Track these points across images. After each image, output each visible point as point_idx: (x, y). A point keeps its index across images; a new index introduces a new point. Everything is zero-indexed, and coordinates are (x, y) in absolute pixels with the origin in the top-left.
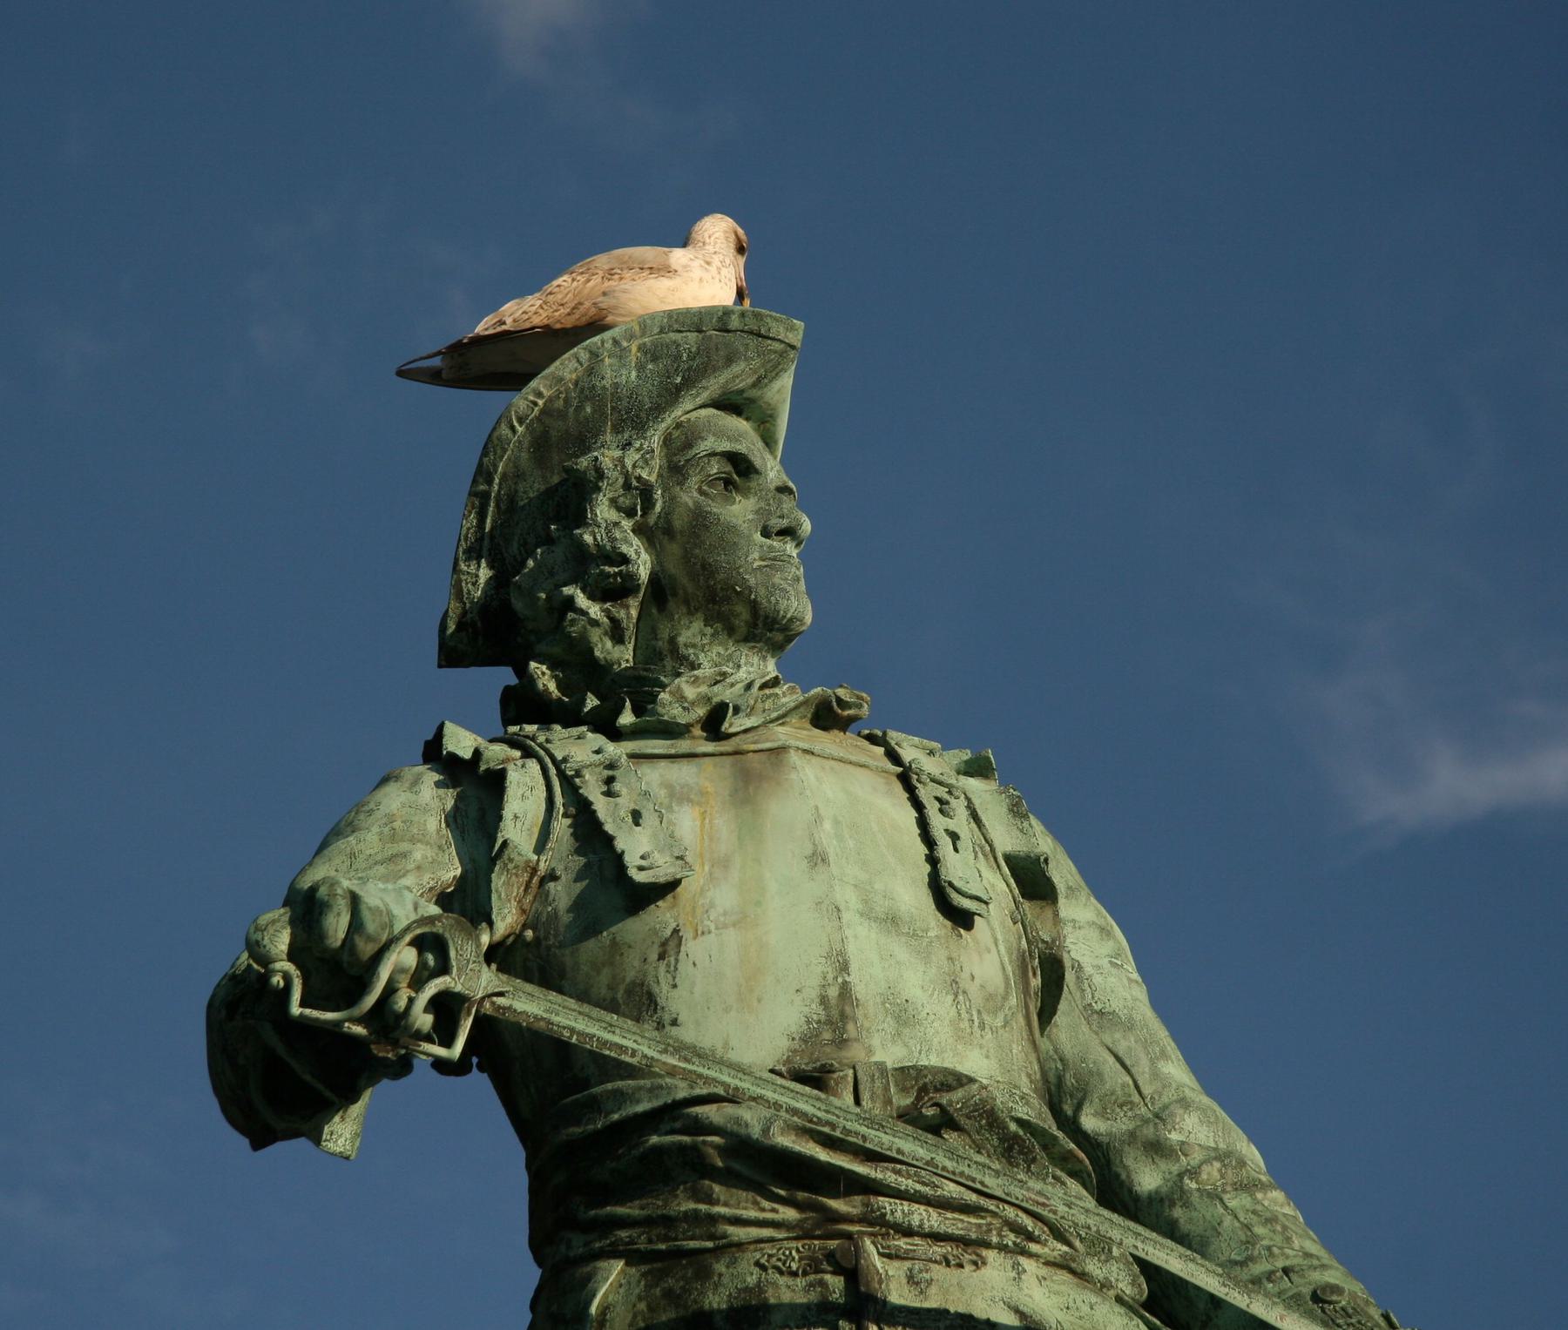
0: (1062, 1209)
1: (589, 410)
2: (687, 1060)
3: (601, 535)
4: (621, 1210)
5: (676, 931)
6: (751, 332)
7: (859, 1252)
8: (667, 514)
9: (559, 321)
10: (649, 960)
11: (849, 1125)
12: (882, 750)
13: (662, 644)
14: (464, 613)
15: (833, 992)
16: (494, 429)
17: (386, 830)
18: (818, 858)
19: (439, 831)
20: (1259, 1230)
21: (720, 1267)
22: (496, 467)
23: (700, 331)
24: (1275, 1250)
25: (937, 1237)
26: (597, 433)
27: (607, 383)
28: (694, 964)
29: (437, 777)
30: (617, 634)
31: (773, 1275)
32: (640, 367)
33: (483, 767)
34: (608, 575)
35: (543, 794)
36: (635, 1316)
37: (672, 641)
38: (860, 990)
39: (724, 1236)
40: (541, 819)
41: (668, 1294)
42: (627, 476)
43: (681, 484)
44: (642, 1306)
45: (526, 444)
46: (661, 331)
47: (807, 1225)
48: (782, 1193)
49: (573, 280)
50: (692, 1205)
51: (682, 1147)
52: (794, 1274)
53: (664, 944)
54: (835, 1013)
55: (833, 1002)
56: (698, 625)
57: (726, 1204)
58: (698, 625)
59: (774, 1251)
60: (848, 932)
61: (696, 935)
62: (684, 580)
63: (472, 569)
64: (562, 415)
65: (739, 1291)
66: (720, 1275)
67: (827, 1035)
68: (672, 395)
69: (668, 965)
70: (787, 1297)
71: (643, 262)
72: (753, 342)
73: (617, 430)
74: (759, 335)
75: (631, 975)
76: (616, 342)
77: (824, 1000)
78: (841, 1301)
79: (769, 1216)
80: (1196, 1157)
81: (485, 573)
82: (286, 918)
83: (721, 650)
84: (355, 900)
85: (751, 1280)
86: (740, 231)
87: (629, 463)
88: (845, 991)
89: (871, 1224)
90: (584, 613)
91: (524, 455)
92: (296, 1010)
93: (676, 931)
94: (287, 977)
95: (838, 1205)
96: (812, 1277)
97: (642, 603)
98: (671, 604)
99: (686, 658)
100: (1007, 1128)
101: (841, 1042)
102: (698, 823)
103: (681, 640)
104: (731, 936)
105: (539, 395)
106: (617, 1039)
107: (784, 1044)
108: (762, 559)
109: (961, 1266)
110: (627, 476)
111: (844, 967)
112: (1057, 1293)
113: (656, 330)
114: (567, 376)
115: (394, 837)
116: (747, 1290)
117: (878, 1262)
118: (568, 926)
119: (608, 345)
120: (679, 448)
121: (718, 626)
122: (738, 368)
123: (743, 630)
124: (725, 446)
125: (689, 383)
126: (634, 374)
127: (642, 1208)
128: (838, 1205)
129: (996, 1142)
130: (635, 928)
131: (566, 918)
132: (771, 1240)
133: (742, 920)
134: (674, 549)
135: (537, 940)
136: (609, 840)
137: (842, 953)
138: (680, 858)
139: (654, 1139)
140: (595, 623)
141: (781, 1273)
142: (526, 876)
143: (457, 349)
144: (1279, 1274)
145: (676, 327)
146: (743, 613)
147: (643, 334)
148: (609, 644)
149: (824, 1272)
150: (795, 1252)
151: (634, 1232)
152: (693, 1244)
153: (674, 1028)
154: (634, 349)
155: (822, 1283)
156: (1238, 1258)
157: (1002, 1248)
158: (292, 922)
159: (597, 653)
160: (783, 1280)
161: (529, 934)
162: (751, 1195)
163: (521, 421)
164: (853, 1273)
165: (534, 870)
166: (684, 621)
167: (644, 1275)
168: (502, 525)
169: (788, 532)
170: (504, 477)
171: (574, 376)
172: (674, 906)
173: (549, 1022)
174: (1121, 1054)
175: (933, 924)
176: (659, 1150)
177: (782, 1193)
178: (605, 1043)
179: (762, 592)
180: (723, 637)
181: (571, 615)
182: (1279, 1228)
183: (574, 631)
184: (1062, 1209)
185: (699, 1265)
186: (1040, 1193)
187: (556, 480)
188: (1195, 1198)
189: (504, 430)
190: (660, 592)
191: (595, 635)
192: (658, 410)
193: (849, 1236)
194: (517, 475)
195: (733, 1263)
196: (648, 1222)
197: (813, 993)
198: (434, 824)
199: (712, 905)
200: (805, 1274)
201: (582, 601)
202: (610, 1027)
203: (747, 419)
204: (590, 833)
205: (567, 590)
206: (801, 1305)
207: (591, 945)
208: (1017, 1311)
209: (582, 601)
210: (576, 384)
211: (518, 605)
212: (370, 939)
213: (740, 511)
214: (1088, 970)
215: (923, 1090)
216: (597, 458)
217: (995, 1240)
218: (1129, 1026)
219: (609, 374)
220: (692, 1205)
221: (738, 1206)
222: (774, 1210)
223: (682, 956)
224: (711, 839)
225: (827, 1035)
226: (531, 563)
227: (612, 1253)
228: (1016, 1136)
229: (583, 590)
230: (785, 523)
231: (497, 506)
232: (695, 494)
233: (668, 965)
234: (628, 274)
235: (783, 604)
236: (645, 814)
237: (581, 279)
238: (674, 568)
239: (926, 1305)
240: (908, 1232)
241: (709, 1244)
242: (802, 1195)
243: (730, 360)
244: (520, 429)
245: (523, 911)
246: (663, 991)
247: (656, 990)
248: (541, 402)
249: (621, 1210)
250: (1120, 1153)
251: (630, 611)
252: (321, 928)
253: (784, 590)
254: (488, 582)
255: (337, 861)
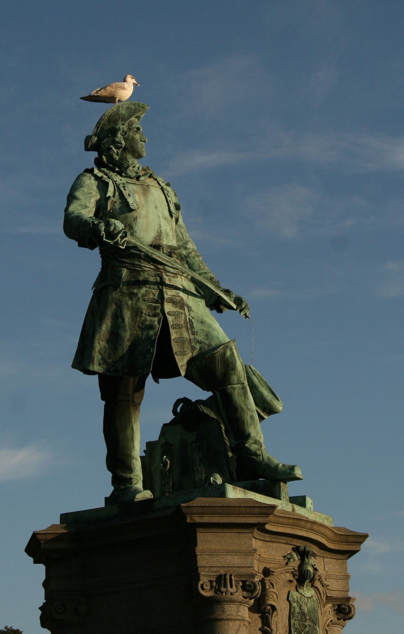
0: (197, 277)
1: (117, 116)
2: (153, 251)
3: (119, 140)
4: (126, 261)
5: (136, 217)
6: (143, 107)
7: (162, 275)
8: (128, 136)
9: (107, 95)
10: (132, 221)
11: (172, 263)
12: (156, 181)
13: (124, 157)
14: (92, 144)
15: (159, 231)
16: (102, 117)
17: (88, 188)
18: (156, 207)
19: (96, 189)
20: (201, 265)
21: (142, 273)
22: (101, 123)
23: (135, 106)
24: (204, 269)
25: (172, 273)
26: (118, 121)
27: (121, 112)
28: (139, 223)
29: (94, 178)
30: (117, 154)
31: (150, 276)
32: (126, 111)
33: (103, 179)
34: (119, 146)
35: (113, 187)
36: (128, 278)
37: (126, 157)
38: (163, 231)
39: (143, 269)
40: (113, 191)
41: (133, 276)
42: (123, 130)
43: (130, 132)
44: (129, 277)
45: (107, 120)
46: (129, 105)
47: (155, 269)
48: (152, 263)
49: (110, 88)
50: (138, 263)
51: (137, 254)
52: (153, 277)
53: (134, 219)
54: (159, 234)
55: (159, 232)
56: (130, 155)
57: (143, 264)
58: (130, 155)
59: (150, 273)
60: (161, 221)
61: (139, 218)
62: (130, 149)
63: (94, 138)
64: (113, 116)
65: (145, 278)
66: (142, 275)
67: (158, 238)
68: (130, 116)
69: (135, 223)
70: (151, 280)
71: (121, 86)
72: (142, 109)
73: (122, 121)
74: (144, 108)
75: (129, 223)
76: (122, 105)
77: (158, 232)
78: (159, 282)
79: (150, 267)
80: (191, 250)
81: (96, 139)
82: (104, 225)
83: (132, 159)
84: (115, 224)
85: (146, 276)
86: (130, 76)
88: (161, 230)
89: (164, 270)
90: (114, 151)
91: (106, 122)
92: (104, 240)
93: (136, 217)
94: (103, 234)
95: (159, 266)
96: (155, 277)
97: (122, 150)
98: (126, 151)
99: (128, 160)
100: (182, 256)
101: (160, 239)
102: (139, 198)
103: (127, 157)
104: (145, 219)
105: (110, 112)
106: (144, 247)
107: (152, 239)
108: (141, 146)
109: (175, 278)
110: (123, 130)
111: (160, 227)
112: (186, 282)
113: (128, 104)
114: (114, 110)
115: (89, 189)
116: (146, 278)
117: (165, 276)
118: (118, 212)
119: (121, 105)
120: (131, 125)
123: (136, 157)
125: (133, 115)
126: (125, 112)
127: (130, 261)
128: (159, 266)
129: (180, 258)
130: (129, 215)
131: (118, 210)
132: (150, 271)
133: (146, 217)
134: (128, 143)
135: (112, 212)
136: (126, 199)
137: (160, 224)
138: (137, 205)
139: (132, 251)
140: (115, 152)
141: (151, 276)
142: (111, 201)
143: (90, 96)
144: (205, 273)
145: (131, 104)
146: (137, 154)
147: (126, 105)
148: (116, 156)
149: (157, 277)
150: (153, 273)
151: (128, 265)
152: (138, 269)
153: (135, 233)
154: (125, 107)
155: (157, 279)
156: (198, 269)
157: (180, 275)
158: (105, 225)
159: (114, 157)
160: (151, 277)
161: (111, 211)
162: (147, 263)
163: (106, 116)
164: (161, 278)
165: (113, 201)
166: (128, 154)
167: (129, 272)
168: (101, 131)
169: (145, 141)
170: (102, 124)
171: (115, 110)
172: (136, 212)
173: (136, 244)
174: (182, 232)
175: (170, 218)
176: (133, 253)
177: (152, 263)
178: (142, 248)
179: (141, 152)
180: (133, 157)
181: (111, 150)
182: (203, 265)
183: (111, 153)
184: (197, 277)
185: (139, 272)
186: (195, 275)
187: (111, 127)
188: (191, 257)
189: (104, 117)
190: (125, 149)
191: (114, 154)
192: (128, 119)
193: (161, 272)
194: (104, 125)
195: (144, 273)
196: (130, 264)
197: (156, 231)
198: (95, 188)
199: (142, 213)
200: (154, 277)
201: (113, 149)
204: (121, 195)
205: (111, 146)
206: (153, 281)
207: (122, 215)
208: (183, 286)
209: (113, 149)
210: (116, 111)
211: (102, 146)
212: (117, 231)
213: (137, 136)
215: (172, 249)
216: (119, 127)
217: (179, 274)
218: (183, 228)
219: (121, 111)
220: (138, 263)
221: (145, 264)
222: (150, 266)
223: (137, 221)
224: (141, 201)
225: (158, 238)
226: (105, 140)
227: (125, 267)
229: (114, 147)
230: (144, 140)
231: (100, 129)
232: (132, 133)
233: (135, 223)
234: (119, 89)
236: (131, 195)
237: (111, 88)
238: (128, 146)
239: (171, 284)
240: (169, 272)
241: (140, 269)
242: (155, 264)
243: (139, 112)
244: (106, 118)
245: (110, 207)
246: (134, 226)
247: (133, 225)
248: (110, 114)
249: (126, 261)
251: (120, 151)
252: (110, 228)
253: (143, 152)
254: (96, 140)
255: (81, 192)
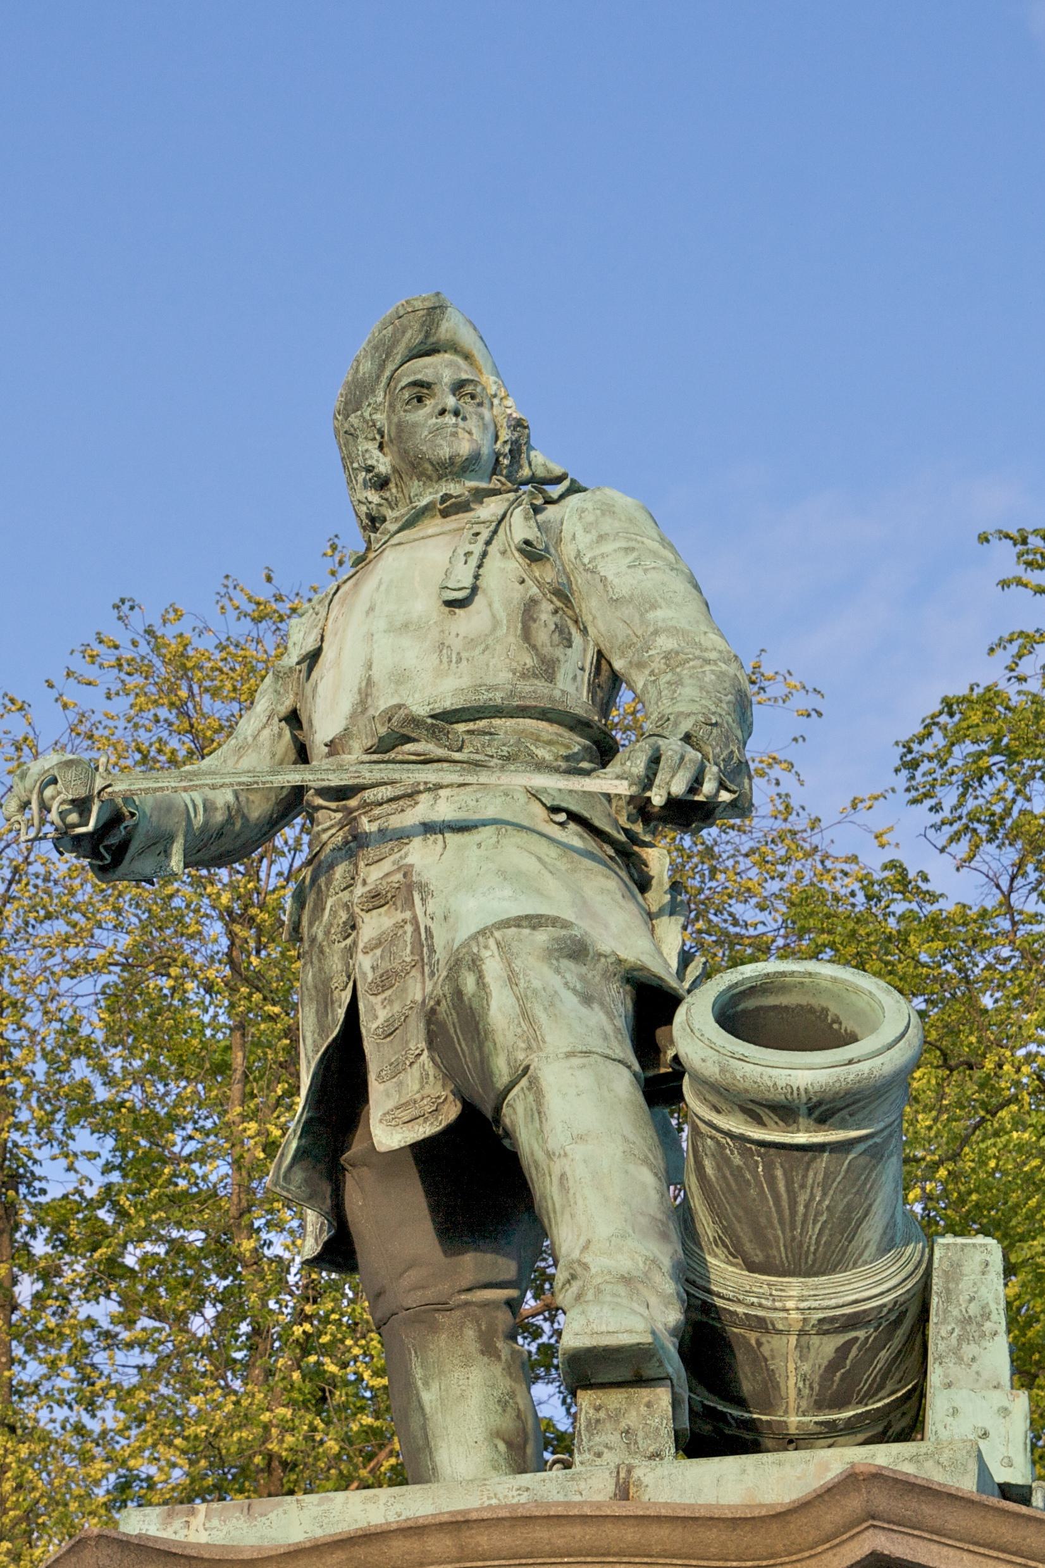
11: (264, 779)
83: (431, 490)
87: (367, 415)
121: (424, 478)
122: (408, 335)
124: (411, 379)
132: (333, 835)
197: (356, 690)
202: (157, 780)
203: (445, 352)
214: (610, 578)
228: (433, 725)
235: (441, 453)
250: (630, 674)
